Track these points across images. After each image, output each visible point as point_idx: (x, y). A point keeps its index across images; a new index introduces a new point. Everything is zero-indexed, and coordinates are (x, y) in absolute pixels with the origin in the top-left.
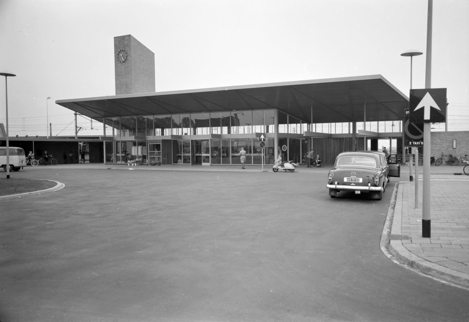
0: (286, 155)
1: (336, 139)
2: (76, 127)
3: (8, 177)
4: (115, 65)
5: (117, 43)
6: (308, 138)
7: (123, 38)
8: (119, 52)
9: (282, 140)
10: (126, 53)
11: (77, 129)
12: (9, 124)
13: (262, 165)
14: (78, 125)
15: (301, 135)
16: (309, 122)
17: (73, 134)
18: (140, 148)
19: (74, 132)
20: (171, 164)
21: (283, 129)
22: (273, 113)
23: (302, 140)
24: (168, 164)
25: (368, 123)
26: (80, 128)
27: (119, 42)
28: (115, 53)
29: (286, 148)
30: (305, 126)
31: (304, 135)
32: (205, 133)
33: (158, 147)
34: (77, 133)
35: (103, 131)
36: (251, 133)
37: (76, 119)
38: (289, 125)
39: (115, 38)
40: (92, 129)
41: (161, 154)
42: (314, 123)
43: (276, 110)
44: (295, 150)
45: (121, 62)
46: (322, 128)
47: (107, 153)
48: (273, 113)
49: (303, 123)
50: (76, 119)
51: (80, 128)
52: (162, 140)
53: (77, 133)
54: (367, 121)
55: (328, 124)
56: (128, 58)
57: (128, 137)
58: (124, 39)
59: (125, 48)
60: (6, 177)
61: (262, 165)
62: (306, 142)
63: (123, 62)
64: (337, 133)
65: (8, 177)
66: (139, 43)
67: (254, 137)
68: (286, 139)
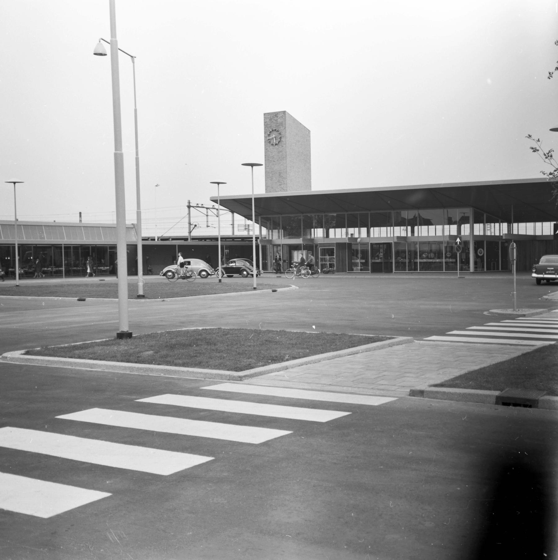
0: (482, 261)
1: (542, 241)
2: (190, 224)
3: (220, 281)
4: (265, 148)
5: (268, 120)
6: (508, 241)
7: (276, 114)
8: (270, 132)
9: (479, 242)
10: (280, 134)
11: (191, 226)
12: (235, 219)
13: (458, 271)
14: (192, 223)
15: (500, 237)
16: (509, 222)
17: (185, 234)
18: (305, 252)
19: (187, 231)
20: (346, 271)
21: (479, 229)
22: (469, 212)
23: (501, 242)
24: (343, 271)
25: (488, 226)
26: (196, 226)
27: (271, 119)
28: (265, 133)
29: (483, 252)
30: (505, 225)
31: (504, 238)
32: (338, 236)
33: (330, 252)
34: (190, 232)
35: (231, 229)
36: (392, 236)
37: (189, 214)
38: (420, 227)
39: (265, 114)
40: (208, 226)
41: (335, 260)
42: (515, 222)
43: (471, 209)
44: (493, 256)
45: (272, 145)
46: (525, 229)
47: (263, 260)
48: (469, 212)
49: (502, 222)
50: (189, 214)
51: (196, 226)
52: (337, 243)
53: (190, 232)
54: (487, 222)
55: (549, 223)
56: (283, 139)
57: (278, 238)
58: (277, 117)
59: (277, 128)
60: (218, 281)
61: (458, 271)
62: (506, 244)
63: (276, 144)
64: (544, 234)
65: (220, 281)
66: (294, 120)
67: (448, 239)
68: (483, 242)
